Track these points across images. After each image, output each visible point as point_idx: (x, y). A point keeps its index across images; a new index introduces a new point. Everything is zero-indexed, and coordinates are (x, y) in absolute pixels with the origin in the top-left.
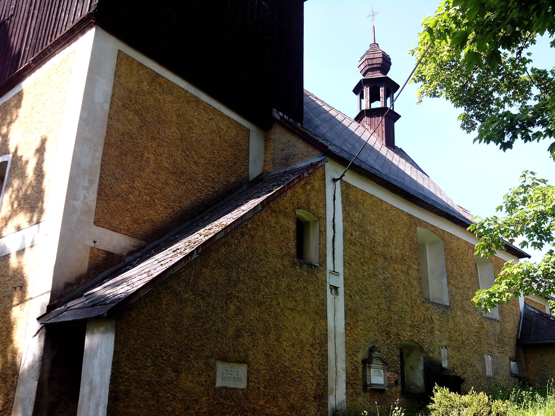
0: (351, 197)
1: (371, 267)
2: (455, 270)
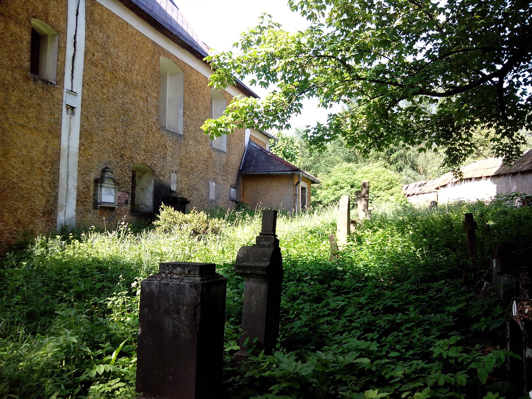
0: (96, 15)
1: (111, 90)
2: (192, 102)
